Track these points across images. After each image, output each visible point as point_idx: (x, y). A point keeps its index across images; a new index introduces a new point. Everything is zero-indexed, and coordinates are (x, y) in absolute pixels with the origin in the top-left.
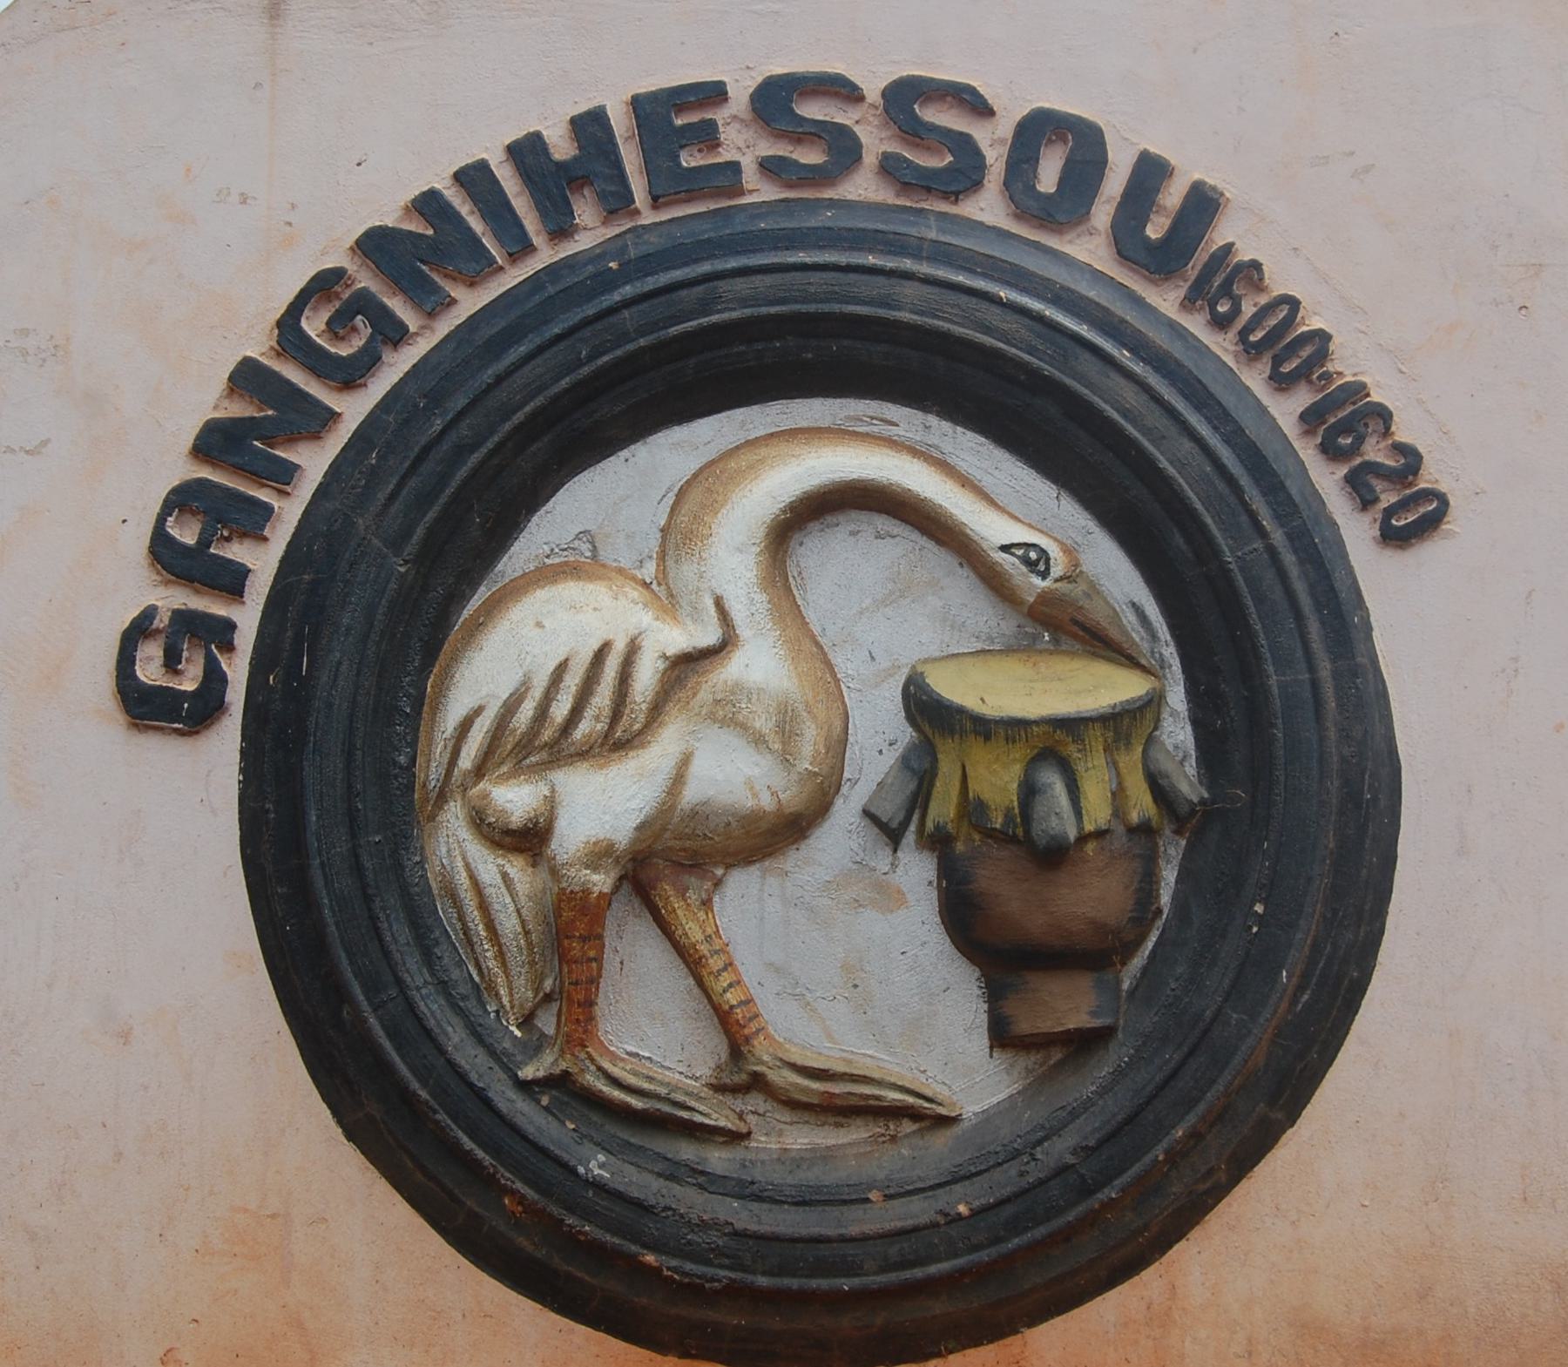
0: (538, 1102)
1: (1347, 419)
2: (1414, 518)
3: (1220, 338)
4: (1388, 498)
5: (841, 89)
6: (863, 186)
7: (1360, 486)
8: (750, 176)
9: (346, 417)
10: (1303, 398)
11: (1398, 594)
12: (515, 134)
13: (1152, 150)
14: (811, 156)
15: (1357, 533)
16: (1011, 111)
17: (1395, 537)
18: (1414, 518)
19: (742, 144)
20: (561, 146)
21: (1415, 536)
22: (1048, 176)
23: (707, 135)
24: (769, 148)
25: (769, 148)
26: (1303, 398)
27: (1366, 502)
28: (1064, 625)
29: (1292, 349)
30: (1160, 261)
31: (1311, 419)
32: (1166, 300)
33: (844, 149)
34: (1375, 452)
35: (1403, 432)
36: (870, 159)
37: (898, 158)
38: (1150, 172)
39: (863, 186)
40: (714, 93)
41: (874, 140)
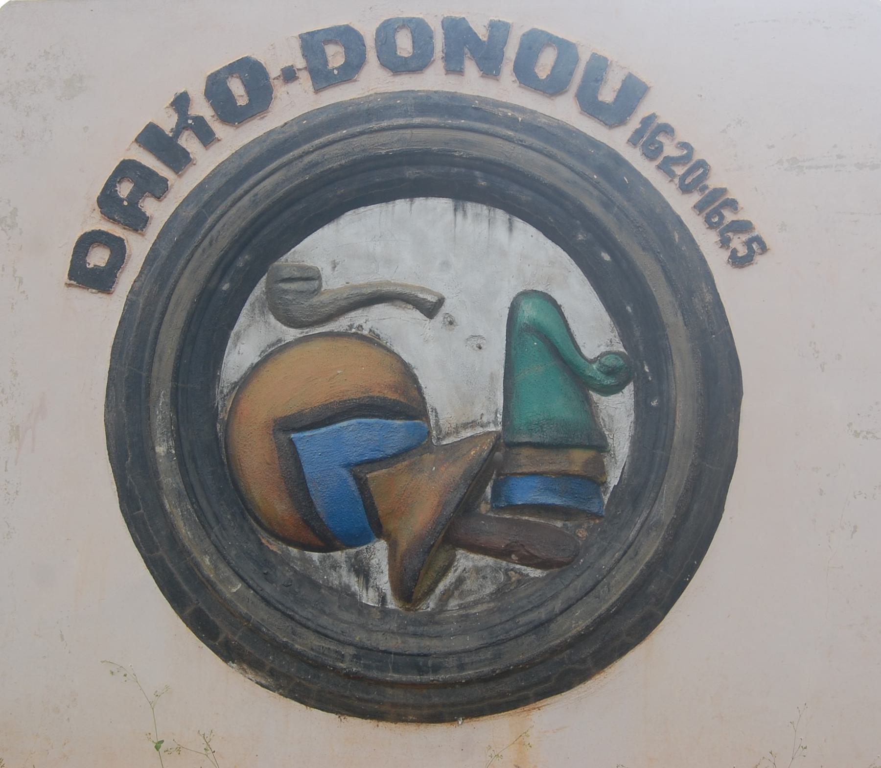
1: (715, 205)
2: (749, 251)
3: (646, 163)
4: (680, 171)
7: (666, 166)
9: (191, 94)
10: (696, 197)
11: (740, 294)
15: (716, 259)
17: (738, 262)
18: (749, 251)
20: (168, 122)
21: (629, 115)
26: (696, 197)
27: (671, 174)
29: (694, 174)
31: (699, 208)
34: (670, 150)
35: (682, 135)
37: (447, 58)
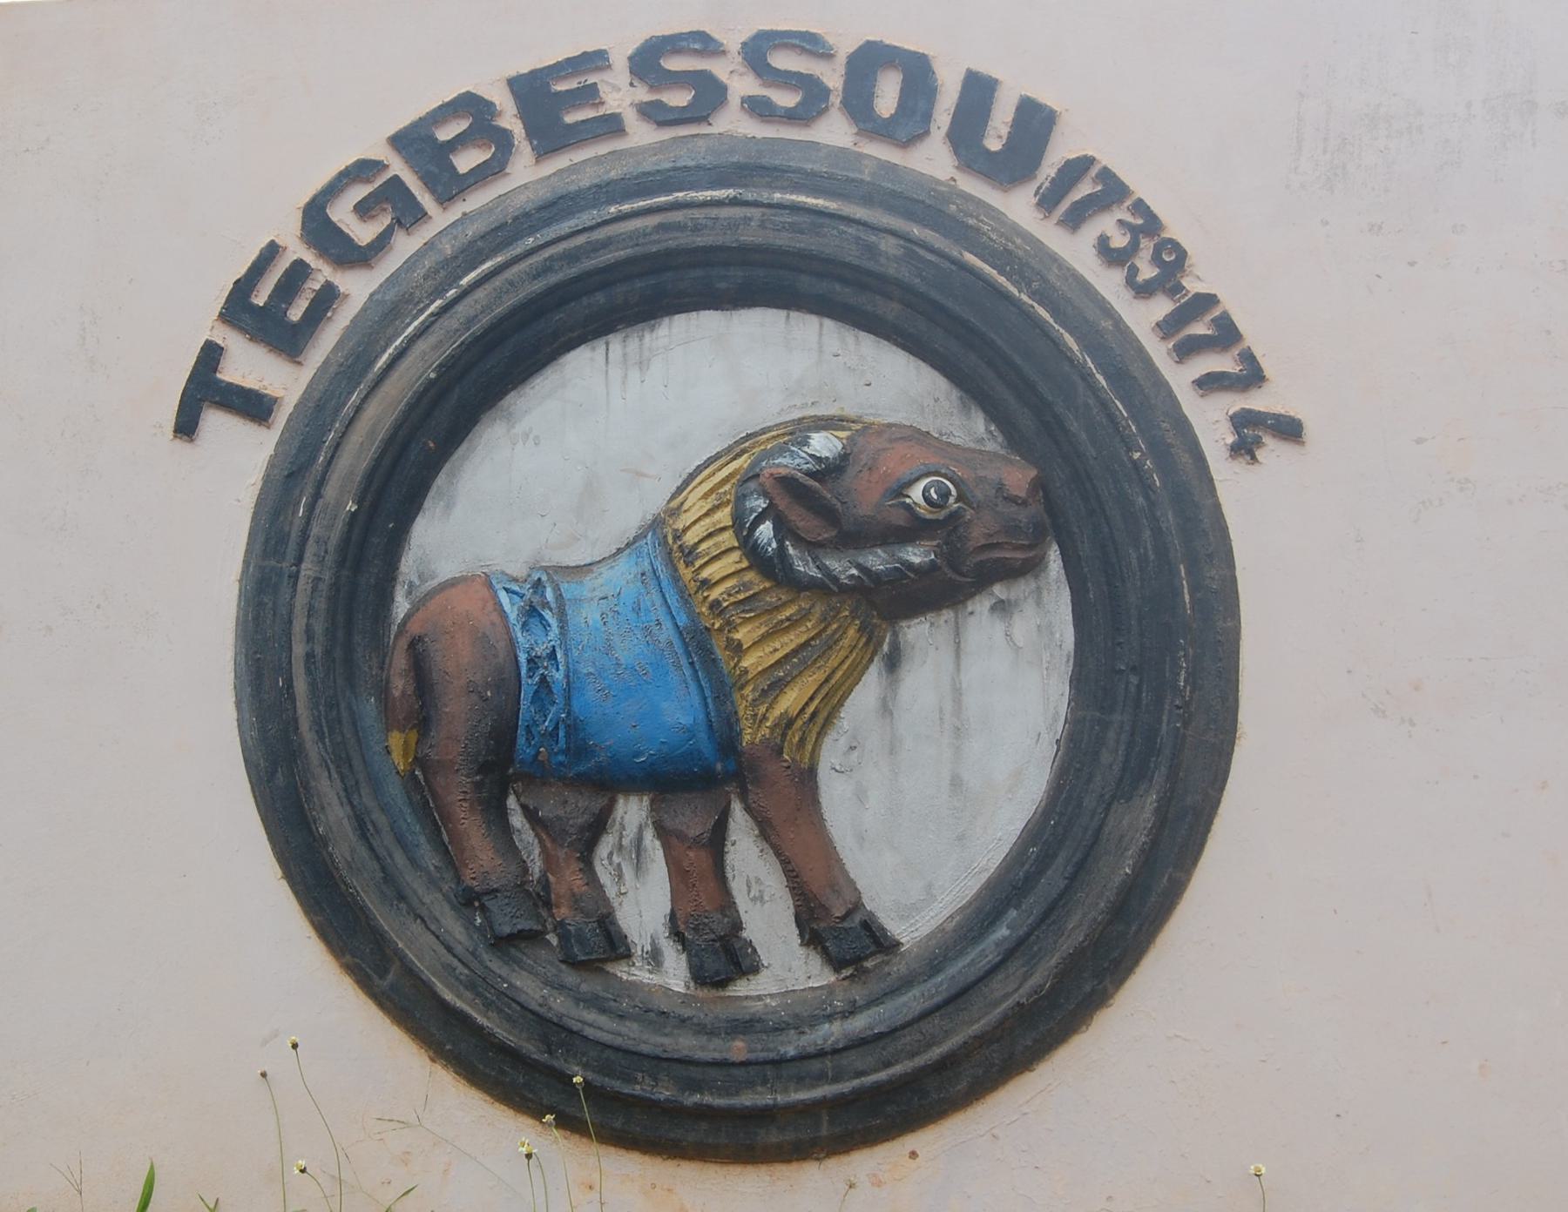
0: (471, 922)
5: (704, 44)
6: (732, 122)
8: (631, 118)
10: (1162, 307)
12: (1047, 97)
13: (630, 52)
14: (786, 99)
16: (845, 46)
19: (620, 93)
22: (887, 95)
23: (589, 94)
24: (643, 94)
25: (643, 94)
26: (1162, 307)
28: (804, 616)
30: (1013, 165)
32: (1018, 207)
33: (710, 94)
36: (734, 99)
38: (979, 90)
39: (732, 122)
40: (595, 60)
41: (742, 85)
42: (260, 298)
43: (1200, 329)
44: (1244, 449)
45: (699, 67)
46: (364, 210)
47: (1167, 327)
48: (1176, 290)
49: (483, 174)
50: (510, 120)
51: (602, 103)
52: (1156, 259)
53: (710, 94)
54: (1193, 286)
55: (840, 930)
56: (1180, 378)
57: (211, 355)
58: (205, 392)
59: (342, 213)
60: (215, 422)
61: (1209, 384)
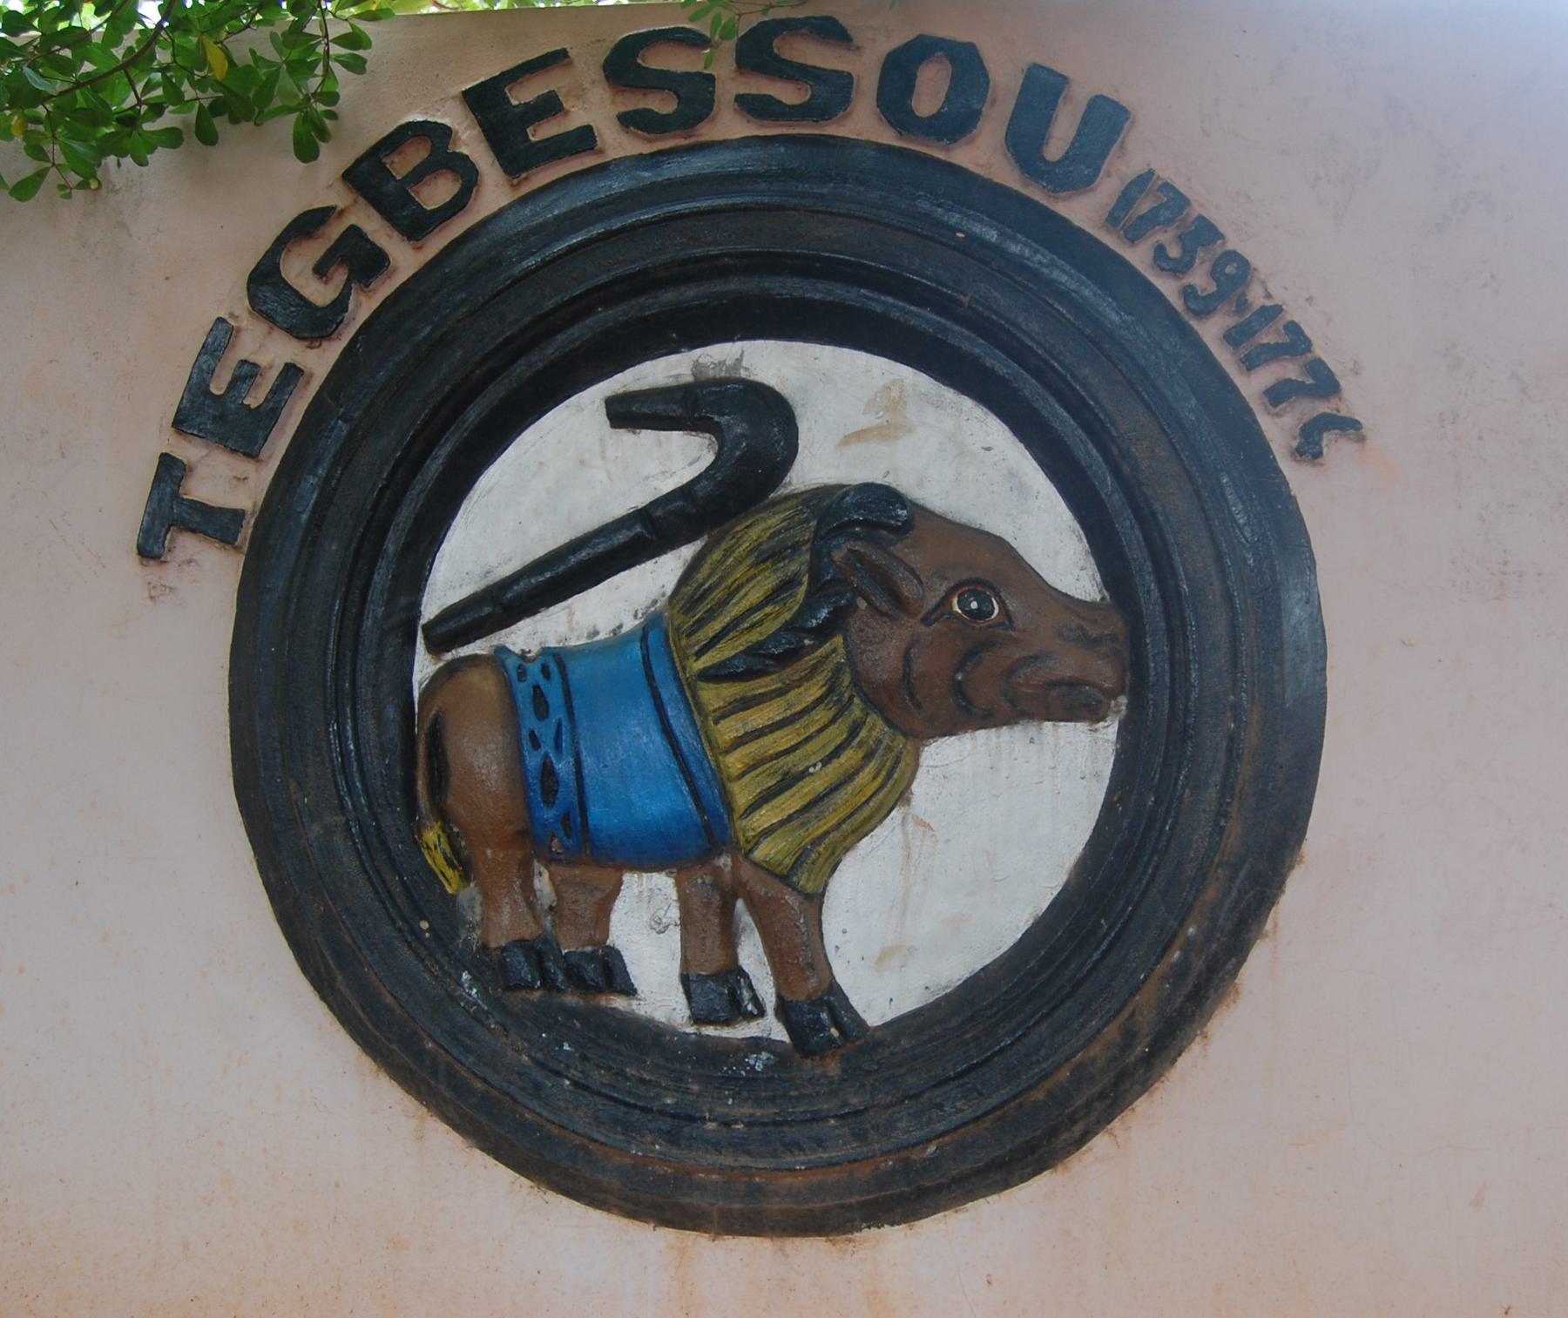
19: (593, 108)
39: (729, 125)
41: (730, 84)
42: (218, 387)
43: (1268, 337)
44: (1309, 448)
45: (641, 106)
46: (321, 270)
47: (1233, 338)
48: (1242, 305)
49: (457, 205)
50: (470, 142)
51: (311, 375)
52: (1215, 273)
53: (696, 97)
54: (1256, 297)
55: (817, 1009)
56: (1251, 386)
57: (170, 470)
58: (170, 516)
59: (298, 269)
60: (187, 545)
61: (1277, 395)
